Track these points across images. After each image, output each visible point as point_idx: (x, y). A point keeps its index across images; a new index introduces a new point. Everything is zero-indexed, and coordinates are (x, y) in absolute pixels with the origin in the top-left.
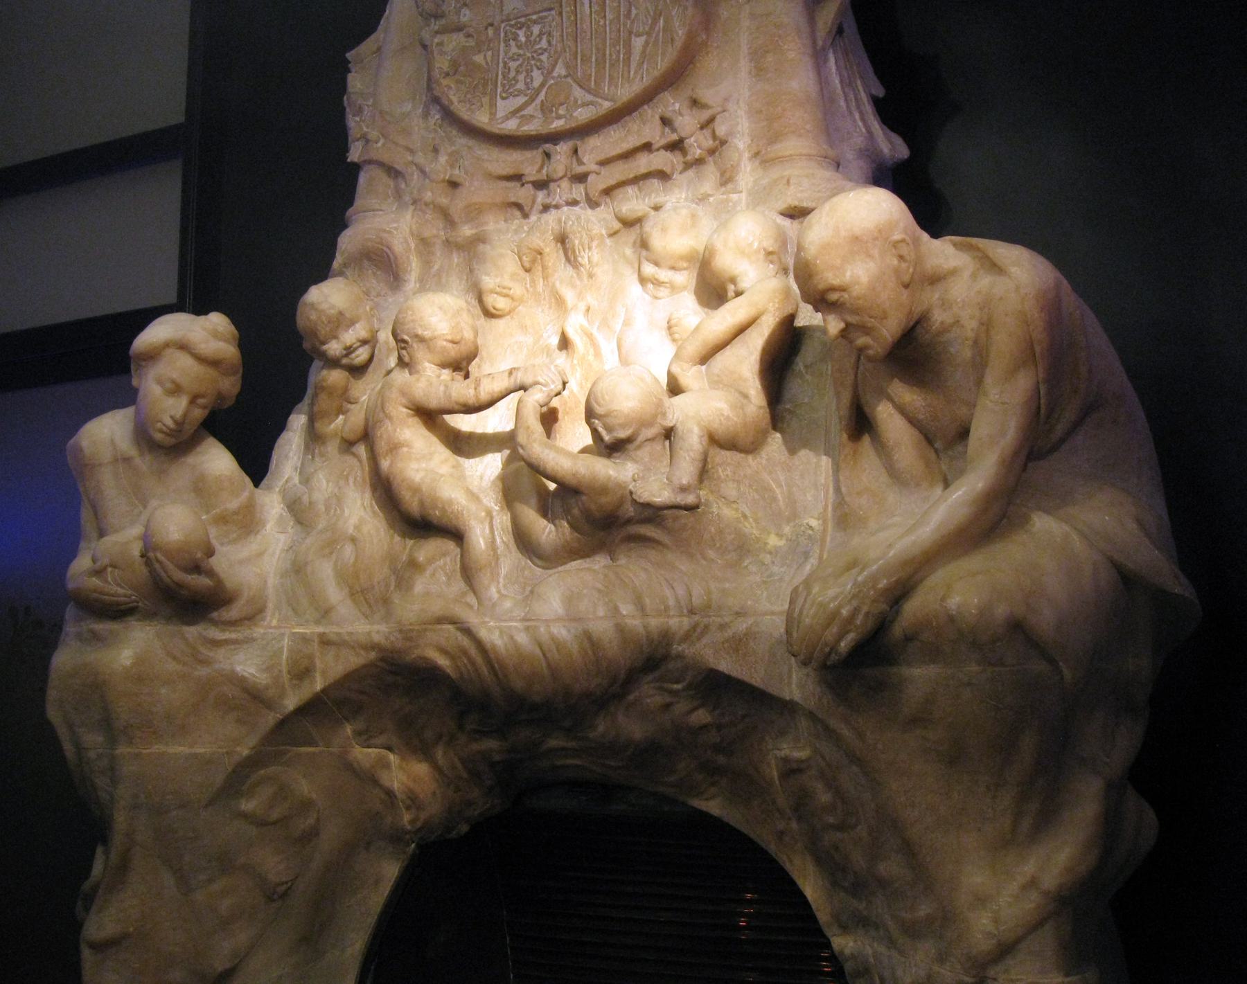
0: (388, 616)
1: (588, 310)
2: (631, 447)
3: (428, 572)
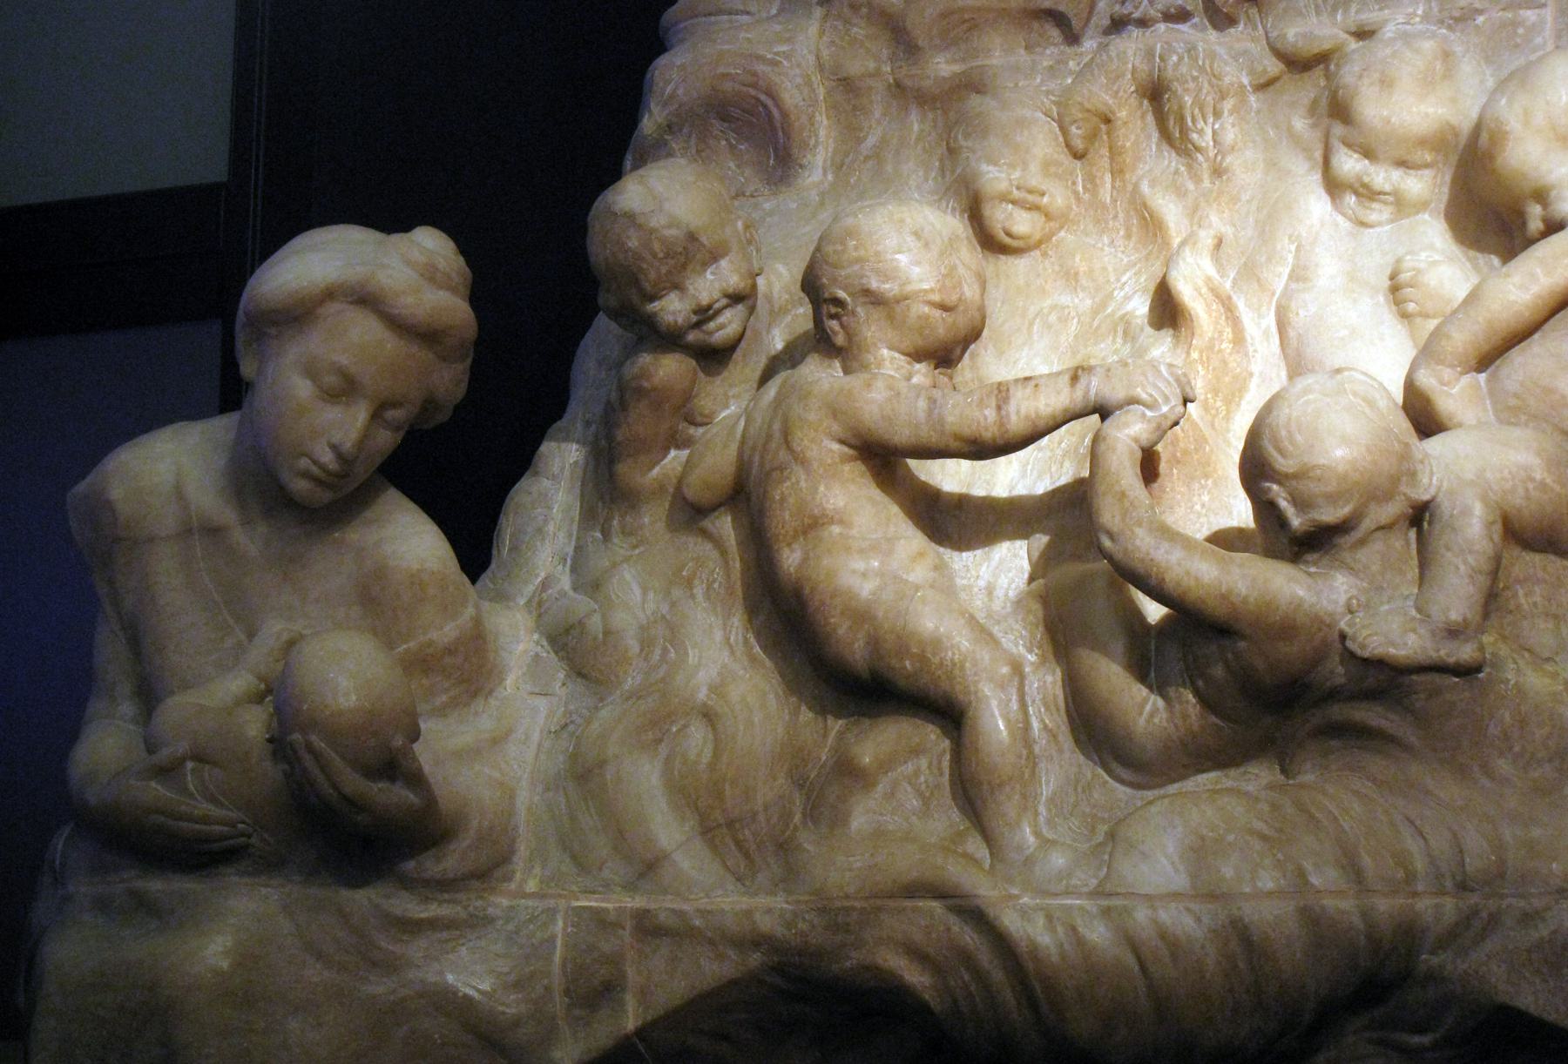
0: (790, 876)
1: (1219, 243)
2: (1346, 541)
3: (880, 788)
